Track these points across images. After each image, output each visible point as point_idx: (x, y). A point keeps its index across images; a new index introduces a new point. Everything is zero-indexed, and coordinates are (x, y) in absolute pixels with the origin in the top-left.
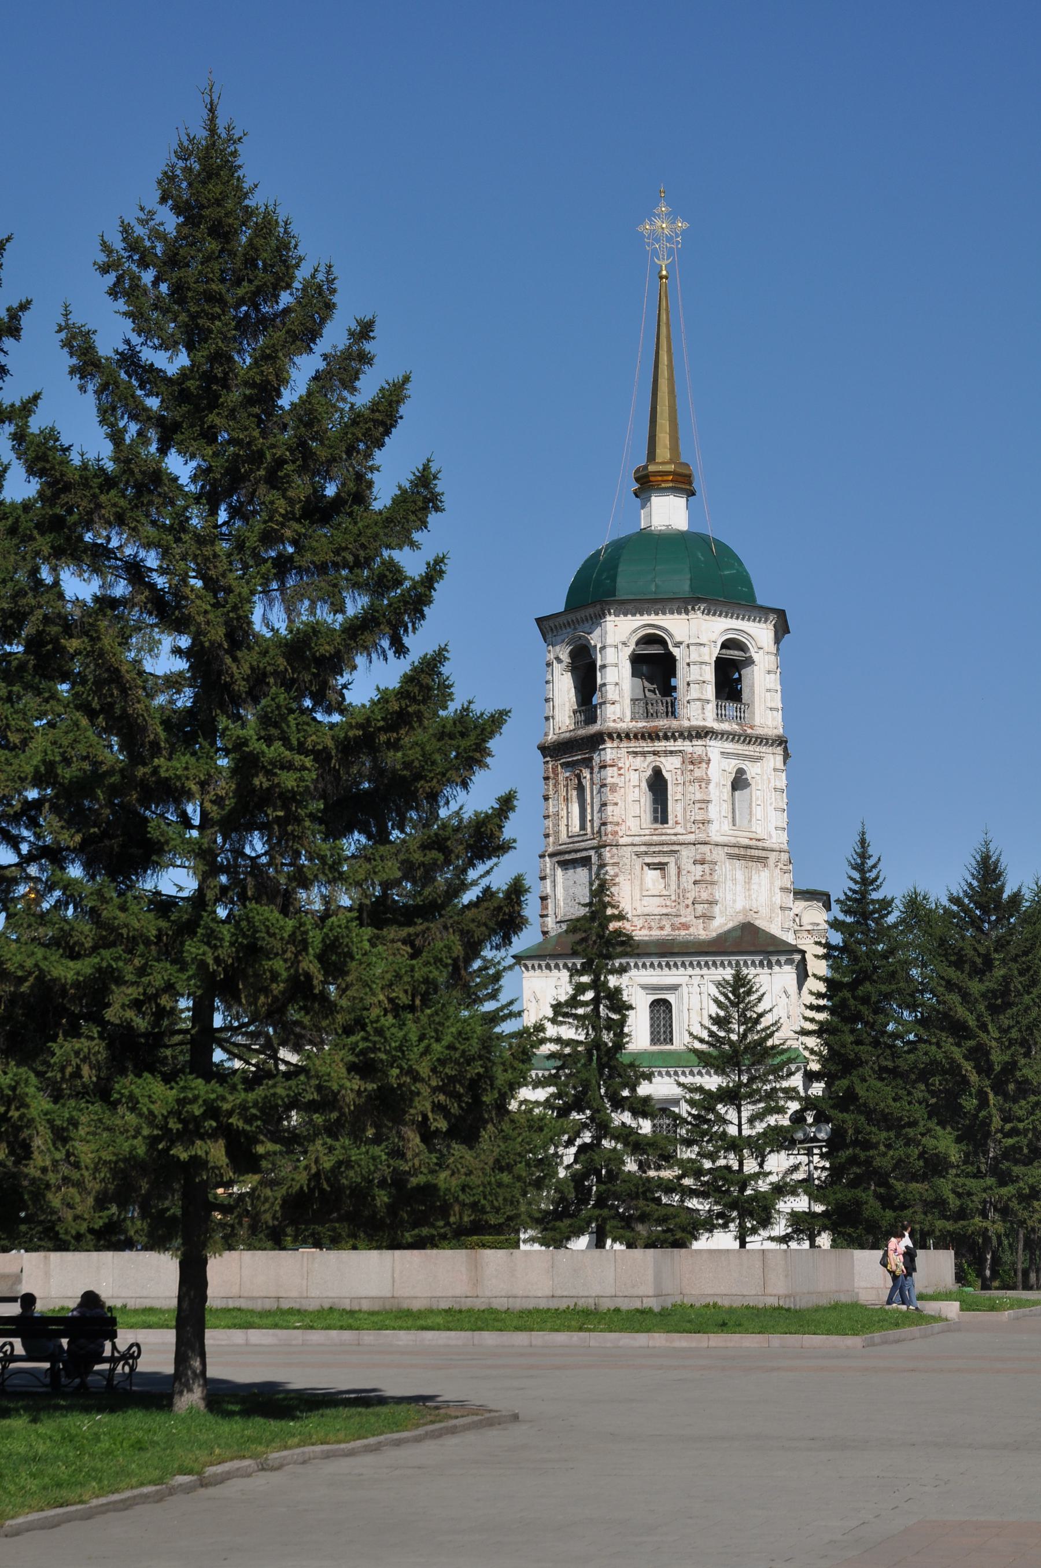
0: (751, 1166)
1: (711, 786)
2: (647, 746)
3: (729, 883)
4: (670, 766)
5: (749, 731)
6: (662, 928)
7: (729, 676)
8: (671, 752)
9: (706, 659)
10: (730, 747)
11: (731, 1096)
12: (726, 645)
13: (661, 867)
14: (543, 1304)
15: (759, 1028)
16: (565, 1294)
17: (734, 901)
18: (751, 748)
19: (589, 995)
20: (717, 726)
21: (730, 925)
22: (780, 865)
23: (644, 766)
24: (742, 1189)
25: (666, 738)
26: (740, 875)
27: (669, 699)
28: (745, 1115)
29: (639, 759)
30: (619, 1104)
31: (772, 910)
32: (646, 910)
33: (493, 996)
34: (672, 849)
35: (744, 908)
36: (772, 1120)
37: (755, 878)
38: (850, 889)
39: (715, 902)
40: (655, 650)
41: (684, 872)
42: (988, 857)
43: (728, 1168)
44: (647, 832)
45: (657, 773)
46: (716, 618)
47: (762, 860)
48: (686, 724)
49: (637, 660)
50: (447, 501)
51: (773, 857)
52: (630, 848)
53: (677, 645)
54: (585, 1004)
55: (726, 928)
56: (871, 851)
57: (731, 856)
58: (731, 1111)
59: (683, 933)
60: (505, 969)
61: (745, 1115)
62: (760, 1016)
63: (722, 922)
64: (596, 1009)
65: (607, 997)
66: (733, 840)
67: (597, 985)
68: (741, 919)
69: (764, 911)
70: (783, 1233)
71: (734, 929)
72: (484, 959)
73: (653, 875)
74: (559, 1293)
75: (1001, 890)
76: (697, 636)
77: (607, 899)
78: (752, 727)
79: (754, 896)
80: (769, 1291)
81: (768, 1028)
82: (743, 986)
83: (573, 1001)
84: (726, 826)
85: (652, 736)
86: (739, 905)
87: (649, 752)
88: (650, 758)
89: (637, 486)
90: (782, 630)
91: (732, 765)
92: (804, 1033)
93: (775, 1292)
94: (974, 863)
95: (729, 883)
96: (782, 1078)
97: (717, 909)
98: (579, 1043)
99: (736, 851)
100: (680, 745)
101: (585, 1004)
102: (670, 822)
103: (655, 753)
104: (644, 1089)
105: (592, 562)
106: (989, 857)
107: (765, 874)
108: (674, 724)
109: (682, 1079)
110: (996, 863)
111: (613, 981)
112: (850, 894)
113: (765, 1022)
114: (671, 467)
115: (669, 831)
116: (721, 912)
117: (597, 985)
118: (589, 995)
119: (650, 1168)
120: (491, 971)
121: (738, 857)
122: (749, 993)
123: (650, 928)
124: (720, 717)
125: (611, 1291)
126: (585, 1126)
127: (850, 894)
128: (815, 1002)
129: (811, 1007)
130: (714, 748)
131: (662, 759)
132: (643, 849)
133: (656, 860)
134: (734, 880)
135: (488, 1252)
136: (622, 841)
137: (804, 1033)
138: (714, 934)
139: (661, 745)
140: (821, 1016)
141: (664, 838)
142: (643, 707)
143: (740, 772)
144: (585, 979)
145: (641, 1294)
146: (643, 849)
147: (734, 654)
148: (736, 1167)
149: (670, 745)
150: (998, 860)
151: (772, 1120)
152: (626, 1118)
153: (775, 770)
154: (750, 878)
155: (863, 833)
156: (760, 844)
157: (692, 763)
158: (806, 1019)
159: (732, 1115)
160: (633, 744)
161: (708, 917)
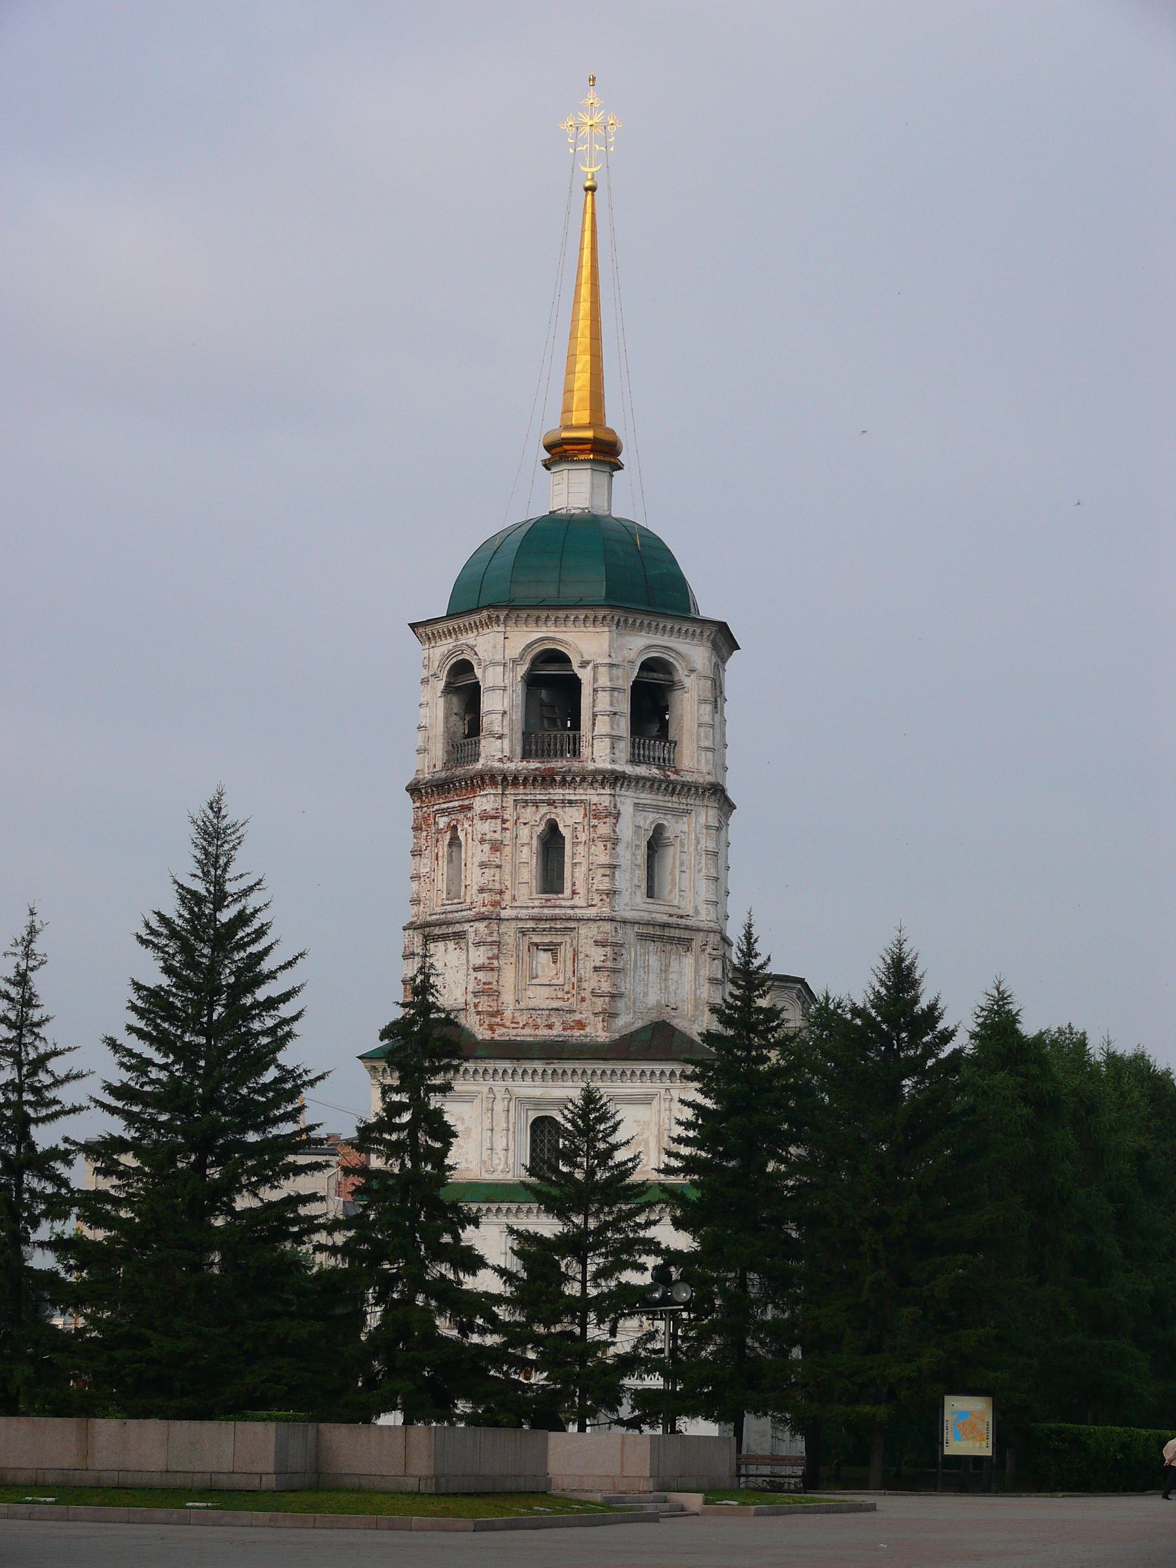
0: (595, 1333)
1: (620, 848)
2: (539, 794)
3: (640, 971)
4: (568, 819)
5: (673, 777)
6: (550, 1027)
8: (570, 802)
9: (620, 683)
10: (646, 797)
11: (576, 1245)
12: (647, 666)
13: (552, 949)
14: (156, 1480)
16: (180, 1469)
17: (646, 994)
18: (675, 799)
19: (406, 1117)
20: (629, 769)
21: (639, 1024)
22: (709, 950)
24: (583, 1364)
25: (563, 783)
26: (654, 961)
28: (591, 1268)
29: (530, 809)
30: (440, 1253)
31: (696, 1007)
32: (532, 1004)
33: (292, 1116)
34: (568, 924)
35: (659, 1003)
37: (674, 966)
39: (621, 995)
40: (552, 670)
41: (581, 956)
42: (901, 960)
43: (571, 1333)
44: (537, 903)
45: (553, 827)
47: (685, 944)
48: (591, 766)
49: (532, 682)
51: (699, 939)
52: (513, 924)
53: (584, 664)
55: (633, 1028)
56: (758, 947)
57: (642, 937)
59: (577, 1033)
60: (304, 1084)
61: (591, 1268)
62: (616, 1147)
63: (627, 1021)
64: (413, 1136)
65: (426, 1120)
66: (646, 916)
67: (418, 1105)
68: (654, 1017)
69: (688, 1008)
71: (643, 1029)
72: (280, 1067)
73: (544, 957)
74: (174, 1467)
75: (915, 1000)
78: (677, 772)
79: (672, 988)
80: (410, 1471)
81: (625, 1163)
82: (595, 1110)
83: (384, 1125)
84: (640, 897)
85: (547, 779)
86: (653, 999)
87: (543, 801)
88: (544, 809)
89: (547, 456)
91: (648, 820)
92: (668, 1171)
93: (416, 1473)
94: (882, 966)
95: (640, 971)
97: (621, 1004)
99: (651, 930)
100: (580, 794)
101: (400, 1128)
102: (567, 892)
103: (551, 803)
104: (469, 1235)
106: (902, 960)
107: (689, 960)
108: (576, 766)
109: (513, 1221)
110: (911, 968)
111: (435, 1101)
112: (730, 1000)
113: (620, 1156)
114: (589, 434)
115: (564, 903)
116: (627, 1007)
118: (406, 1117)
120: (288, 1086)
121: (652, 938)
122: (603, 1118)
123: (536, 1027)
124: (634, 760)
125: (227, 1467)
126: (397, 1277)
127: (730, 1000)
128: (684, 1134)
129: (679, 1140)
130: (627, 801)
131: (559, 811)
132: (531, 924)
133: (547, 940)
134: (647, 968)
135: (100, 1422)
136: (505, 914)
137: (668, 1171)
138: (617, 1036)
139: (557, 793)
140: (685, 1151)
141: (557, 911)
142: (532, 743)
143: (659, 829)
144: (404, 1098)
145: (260, 1470)
146: (531, 924)
149: (569, 794)
150: (913, 964)
152: (444, 1269)
153: (708, 827)
154: (668, 966)
155: (750, 926)
156: (683, 922)
157: (595, 817)
158: (670, 1154)
159: (575, 1269)
160: (521, 790)
161: (610, 1015)
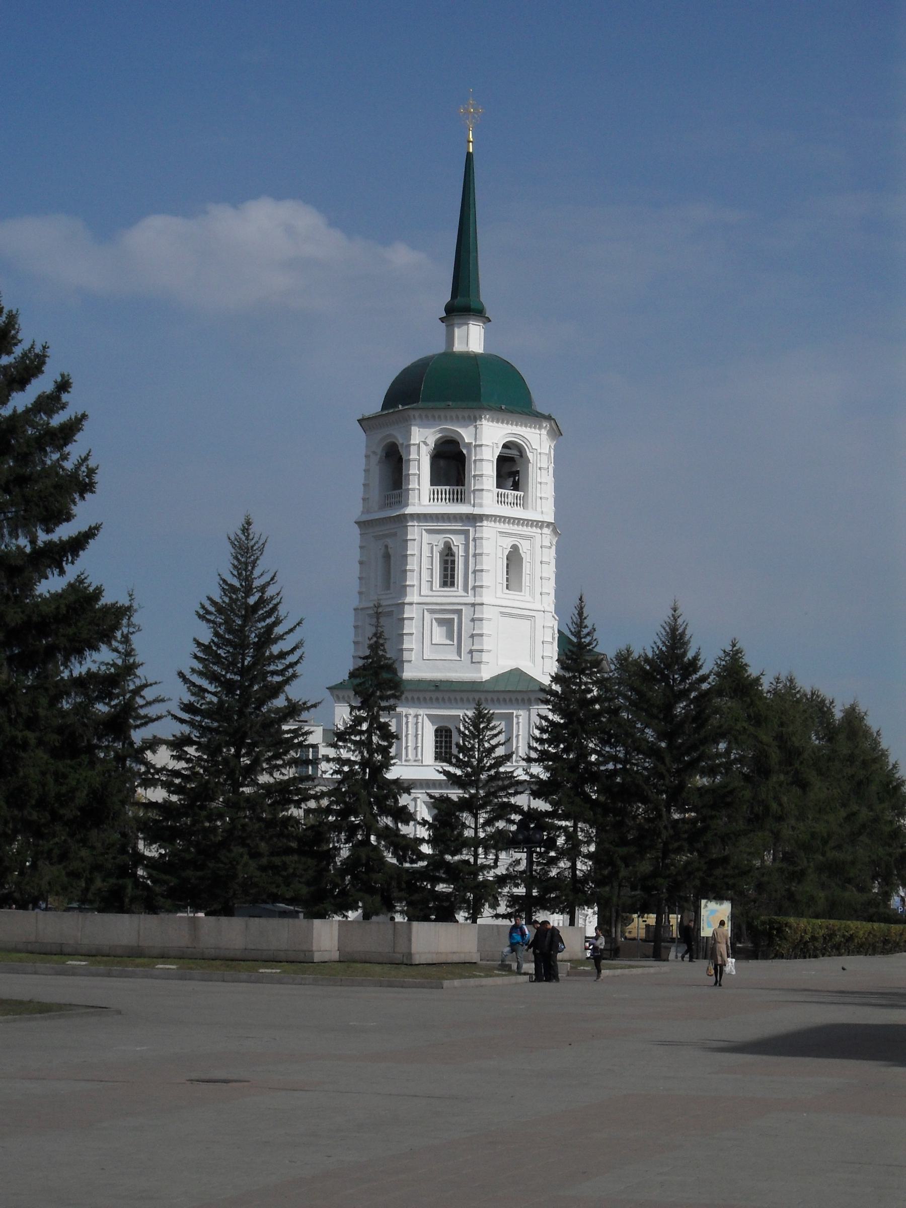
4: (457, 541)
7: (511, 468)
11: (469, 805)
15: (493, 755)
19: (365, 727)
23: (439, 541)
27: (459, 488)
36: (501, 824)
38: (570, 651)
46: (500, 425)
50: (98, 488)
54: (361, 733)
58: (470, 818)
67: (374, 719)
70: (506, 912)
76: (488, 437)
77: (381, 653)
90: (556, 433)
91: (508, 543)
96: (511, 794)
98: (355, 762)
101: (361, 733)
105: (406, 372)
110: (683, 634)
117: (374, 719)
119: (406, 862)
147: (513, 453)
148: (472, 860)
150: (683, 633)
151: (501, 824)
152: (388, 821)
